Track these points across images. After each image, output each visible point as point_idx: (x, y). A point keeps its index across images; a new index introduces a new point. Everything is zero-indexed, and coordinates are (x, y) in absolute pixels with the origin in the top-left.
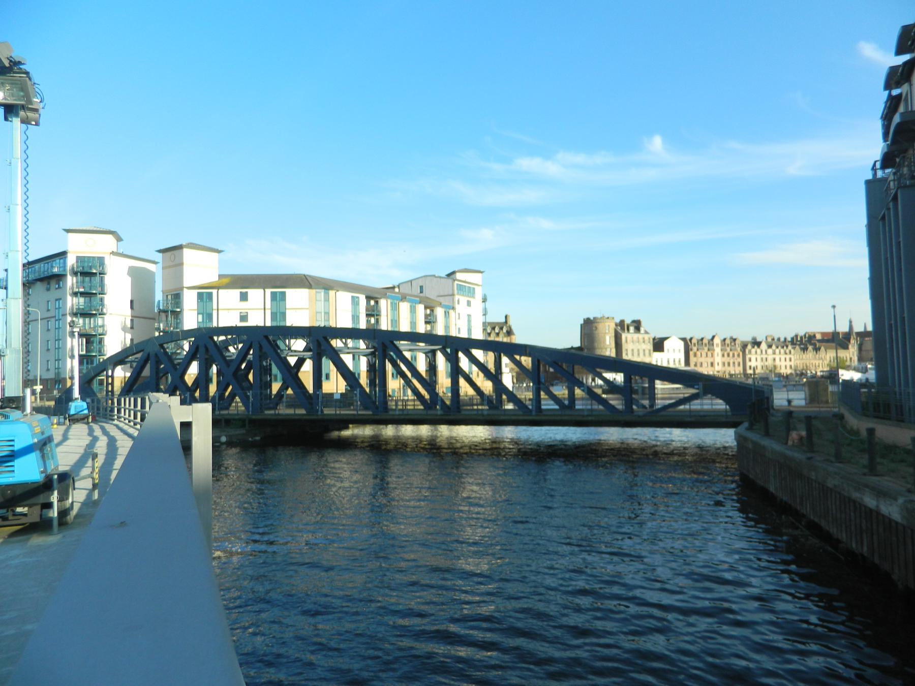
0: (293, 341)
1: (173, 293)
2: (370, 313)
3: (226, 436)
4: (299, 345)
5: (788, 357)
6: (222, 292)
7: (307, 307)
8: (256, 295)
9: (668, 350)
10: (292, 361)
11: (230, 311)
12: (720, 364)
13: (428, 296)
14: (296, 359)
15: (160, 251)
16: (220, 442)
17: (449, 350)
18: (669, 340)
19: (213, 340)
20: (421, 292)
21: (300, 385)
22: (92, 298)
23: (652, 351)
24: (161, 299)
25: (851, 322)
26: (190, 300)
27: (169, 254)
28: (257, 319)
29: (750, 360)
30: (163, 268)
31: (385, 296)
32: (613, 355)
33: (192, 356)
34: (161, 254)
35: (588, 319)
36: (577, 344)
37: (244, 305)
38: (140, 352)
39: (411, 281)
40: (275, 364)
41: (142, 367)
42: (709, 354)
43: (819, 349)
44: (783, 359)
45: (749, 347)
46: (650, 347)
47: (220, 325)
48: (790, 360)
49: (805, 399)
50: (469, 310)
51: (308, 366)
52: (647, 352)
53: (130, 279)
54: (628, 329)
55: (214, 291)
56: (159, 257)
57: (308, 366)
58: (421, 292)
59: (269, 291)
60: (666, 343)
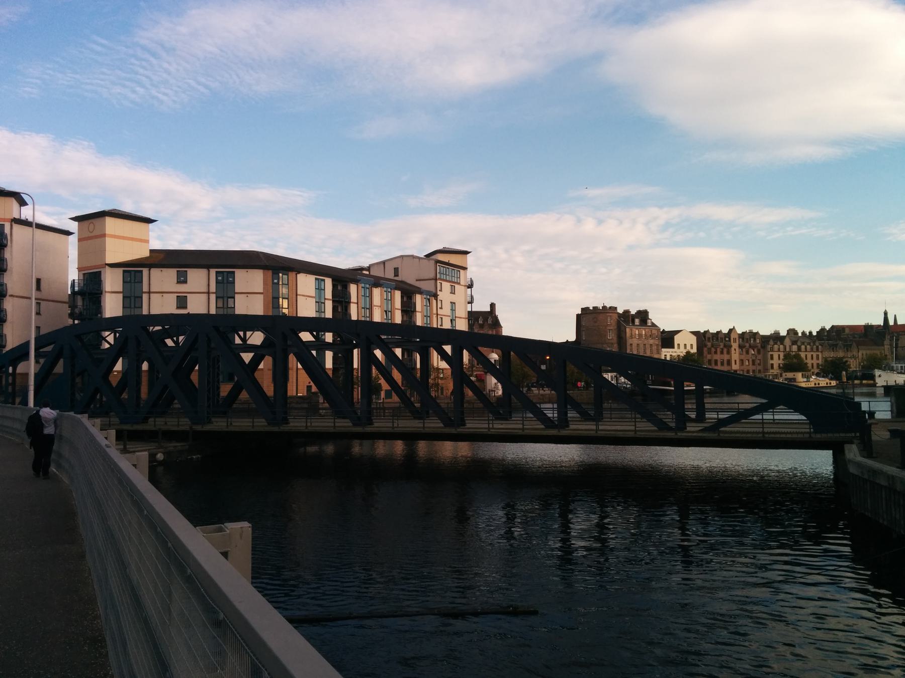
0: (249, 334)
1: (86, 272)
2: (405, 309)
3: (164, 453)
4: (257, 338)
5: (815, 354)
6: (155, 272)
7: (262, 291)
8: (198, 279)
9: (679, 345)
10: (247, 357)
11: (164, 295)
12: (738, 362)
13: (404, 279)
14: (251, 355)
15: (75, 219)
16: (156, 461)
17: (315, 333)
18: (681, 332)
19: (148, 330)
20: (396, 275)
21: (257, 388)
22: (106, 290)
23: (660, 347)
24: (76, 278)
25: (895, 315)
26: (112, 282)
27: (86, 223)
28: (197, 306)
29: (772, 358)
30: (80, 240)
31: (356, 282)
32: (615, 348)
33: (118, 350)
34: (77, 223)
35: (588, 308)
36: (572, 337)
37: (182, 288)
38: (50, 344)
39: (384, 263)
40: (751, 417)
41: (54, 364)
42: (725, 350)
43: (850, 346)
44: (809, 357)
45: (771, 342)
46: (658, 342)
47: (153, 312)
48: (818, 358)
49: (892, 411)
50: (453, 298)
51: (265, 365)
52: (654, 348)
53: (769, 334)
54: (633, 322)
55: (145, 271)
56: (73, 226)
57: (265, 365)
58: (396, 275)
59: (213, 272)
60: (676, 337)
